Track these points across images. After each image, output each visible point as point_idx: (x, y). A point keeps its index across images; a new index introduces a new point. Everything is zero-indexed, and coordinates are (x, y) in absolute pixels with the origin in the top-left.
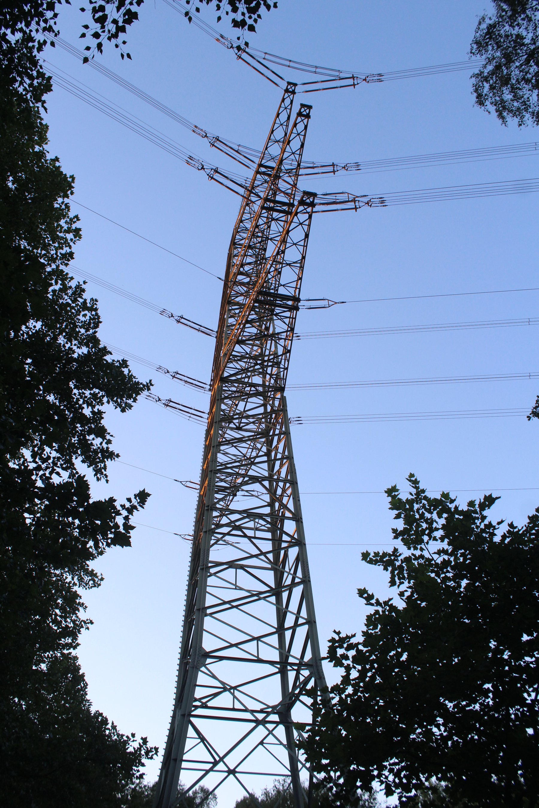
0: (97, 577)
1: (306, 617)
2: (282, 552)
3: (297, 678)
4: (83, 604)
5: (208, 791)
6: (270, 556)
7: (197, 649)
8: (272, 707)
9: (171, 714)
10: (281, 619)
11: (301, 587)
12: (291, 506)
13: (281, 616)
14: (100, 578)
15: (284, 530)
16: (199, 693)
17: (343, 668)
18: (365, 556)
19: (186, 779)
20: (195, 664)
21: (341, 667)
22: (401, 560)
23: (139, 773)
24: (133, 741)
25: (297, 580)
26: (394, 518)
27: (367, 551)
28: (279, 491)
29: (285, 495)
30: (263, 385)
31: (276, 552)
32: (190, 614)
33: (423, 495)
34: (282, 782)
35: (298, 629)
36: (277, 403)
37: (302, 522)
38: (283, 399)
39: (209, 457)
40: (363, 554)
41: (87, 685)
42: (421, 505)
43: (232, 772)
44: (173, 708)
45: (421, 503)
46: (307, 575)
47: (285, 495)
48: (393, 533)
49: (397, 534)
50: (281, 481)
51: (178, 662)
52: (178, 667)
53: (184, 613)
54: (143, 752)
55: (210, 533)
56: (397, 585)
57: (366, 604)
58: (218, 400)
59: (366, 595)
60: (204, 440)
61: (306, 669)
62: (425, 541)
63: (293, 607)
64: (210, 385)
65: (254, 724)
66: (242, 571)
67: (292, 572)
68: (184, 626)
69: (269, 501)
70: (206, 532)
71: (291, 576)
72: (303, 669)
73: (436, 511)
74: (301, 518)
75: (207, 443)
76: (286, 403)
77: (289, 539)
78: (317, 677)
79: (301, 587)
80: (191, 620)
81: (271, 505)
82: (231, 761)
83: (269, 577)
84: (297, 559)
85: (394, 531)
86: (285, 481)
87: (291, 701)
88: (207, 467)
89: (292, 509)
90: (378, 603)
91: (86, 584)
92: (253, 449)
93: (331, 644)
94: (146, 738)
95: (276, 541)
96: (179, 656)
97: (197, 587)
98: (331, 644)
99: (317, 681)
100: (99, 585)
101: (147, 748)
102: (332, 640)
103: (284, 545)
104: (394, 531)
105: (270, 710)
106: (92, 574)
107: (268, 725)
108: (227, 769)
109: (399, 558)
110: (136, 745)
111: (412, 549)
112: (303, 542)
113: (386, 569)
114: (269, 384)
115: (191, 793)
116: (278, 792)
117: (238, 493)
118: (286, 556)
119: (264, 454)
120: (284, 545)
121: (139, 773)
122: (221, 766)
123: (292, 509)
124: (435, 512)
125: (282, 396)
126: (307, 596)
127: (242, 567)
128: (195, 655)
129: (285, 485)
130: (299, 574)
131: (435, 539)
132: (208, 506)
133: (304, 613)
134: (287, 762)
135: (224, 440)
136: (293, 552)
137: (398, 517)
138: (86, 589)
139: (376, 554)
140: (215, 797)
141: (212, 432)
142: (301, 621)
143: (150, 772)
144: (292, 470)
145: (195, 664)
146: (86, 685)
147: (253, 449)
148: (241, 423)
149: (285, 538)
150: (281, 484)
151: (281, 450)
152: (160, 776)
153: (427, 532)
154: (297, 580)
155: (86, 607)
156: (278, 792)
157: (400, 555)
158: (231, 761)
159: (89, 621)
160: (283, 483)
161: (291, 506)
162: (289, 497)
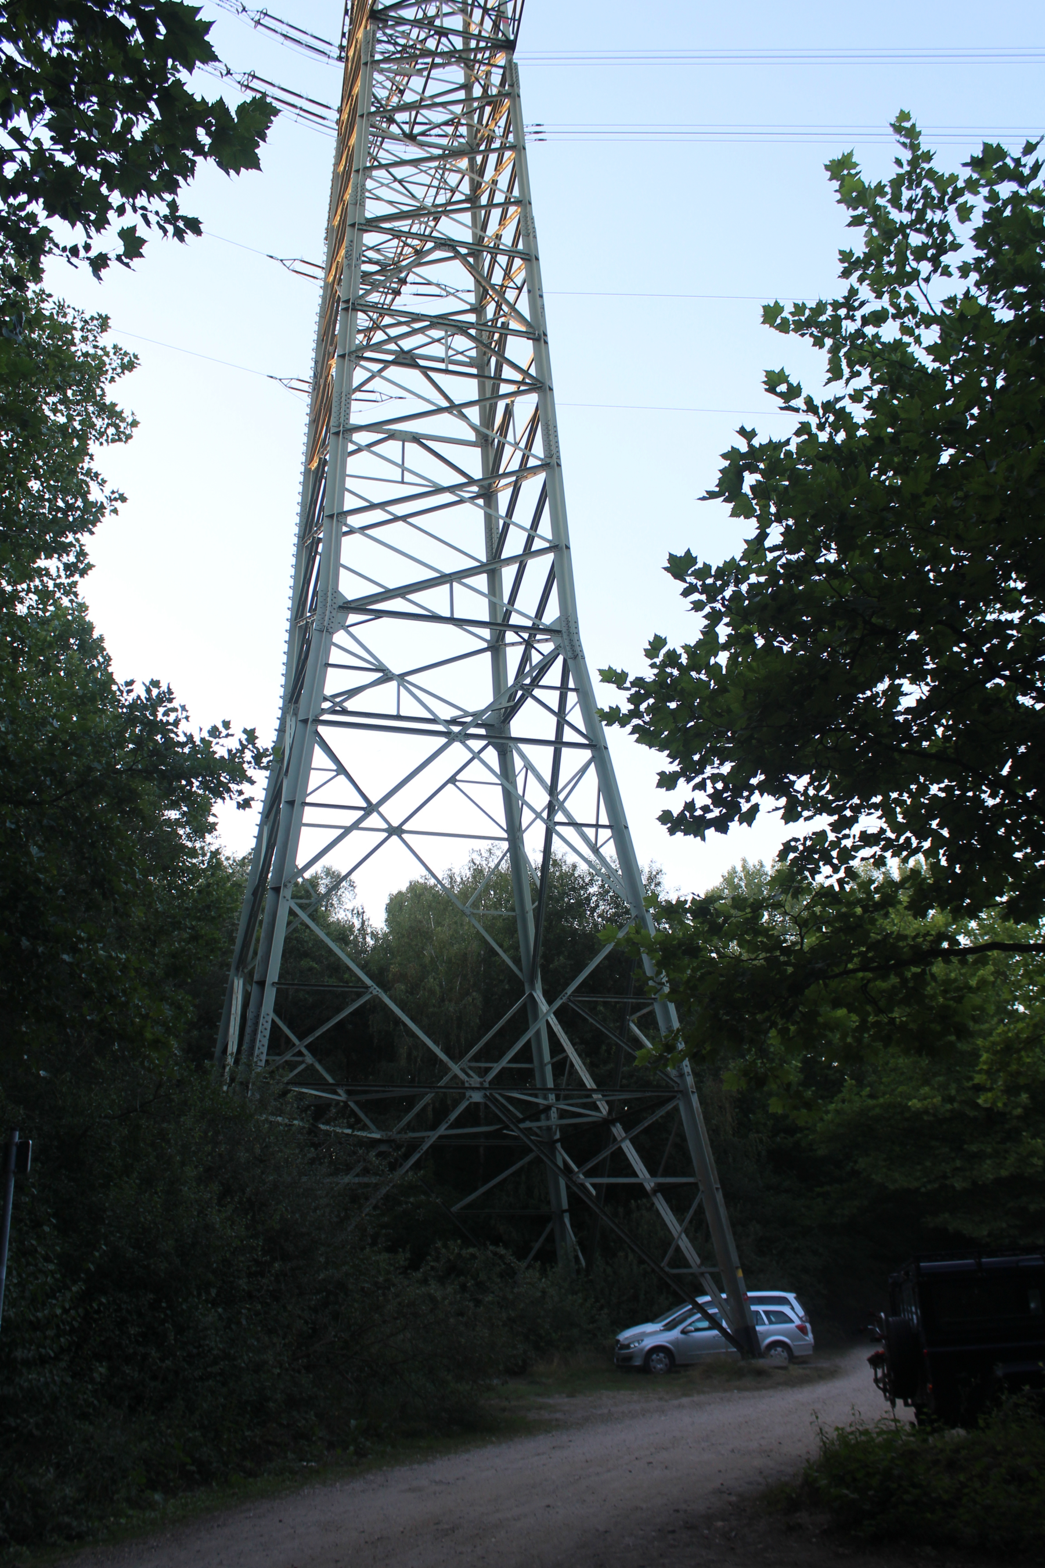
0: (123, 420)
1: (550, 537)
2: (501, 406)
3: (526, 658)
4: (97, 475)
5: (339, 875)
7: (329, 594)
8: (473, 715)
9: (276, 724)
10: (495, 546)
11: (541, 477)
12: (523, 306)
13: (496, 539)
14: (130, 420)
16: (335, 682)
17: (754, 520)
18: (771, 314)
19: (308, 845)
20: (326, 624)
21: (747, 517)
22: (863, 317)
23: (243, 797)
24: (228, 735)
25: (532, 462)
26: (849, 225)
27: (776, 303)
28: (497, 278)
30: (466, 34)
31: (487, 404)
32: (311, 528)
33: (926, 166)
34: (486, 854)
35: (532, 564)
36: (496, 79)
38: (511, 69)
39: (347, 197)
40: (766, 308)
41: (110, 659)
42: (919, 191)
43: (395, 831)
44: (279, 713)
45: (918, 185)
46: (554, 451)
47: (511, 285)
48: (842, 261)
49: (850, 264)
50: (504, 252)
51: (287, 625)
52: (286, 636)
53: (296, 530)
54: (248, 755)
55: (353, 358)
56: (845, 378)
57: (781, 409)
58: (366, 64)
59: (783, 388)
60: (333, 161)
61: (546, 640)
62: (924, 275)
63: (524, 514)
64: (341, 48)
65: (443, 740)
66: (415, 446)
67: (522, 445)
68: (298, 556)
72: (539, 641)
73: (954, 206)
74: (545, 335)
75: (341, 168)
76: (518, 80)
77: (519, 377)
78: (570, 654)
79: (541, 477)
80: (312, 542)
81: (478, 309)
82: (394, 811)
83: (472, 462)
84: (534, 421)
85: (845, 256)
86: (512, 254)
87: (512, 704)
88: (343, 221)
90: (811, 407)
91: (102, 434)
92: (438, 188)
93: (727, 463)
94: (253, 731)
96: (288, 614)
97: (322, 477)
98: (727, 463)
99: (569, 661)
100: (129, 437)
101: (257, 749)
102: (732, 455)
103: (505, 389)
104: (845, 256)
105: (469, 719)
106: (111, 412)
107: (471, 743)
108: (385, 826)
109: (858, 314)
110: (233, 744)
111: (886, 296)
112: (548, 383)
113: (819, 343)
114: (480, 32)
115: (307, 875)
116: (478, 872)
117: (404, 289)
118: (509, 412)
119: (463, 197)
120: (505, 389)
121: (243, 797)
122: (374, 820)
124: (952, 208)
125: (510, 61)
126: (552, 495)
128: (325, 606)
129: (510, 264)
130: (538, 448)
131: (946, 272)
132: (347, 301)
133: (545, 528)
134: (500, 814)
135: (376, 163)
136: (525, 406)
137: (856, 221)
138: (101, 444)
139: (799, 309)
140: (352, 886)
141: (352, 141)
142: (538, 544)
143: (233, 831)
144: (526, 229)
145: (326, 624)
146: (108, 659)
147: (438, 188)
148: (415, 123)
149: (508, 373)
150: (503, 260)
151: (503, 182)
152: (259, 838)
153: (930, 253)
154: (532, 462)
155: (104, 481)
156: (478, 872)
157: (862, 304)
158: (394, 811)
159: (116, 495)
160: (506, 259)
161: (523, 306)
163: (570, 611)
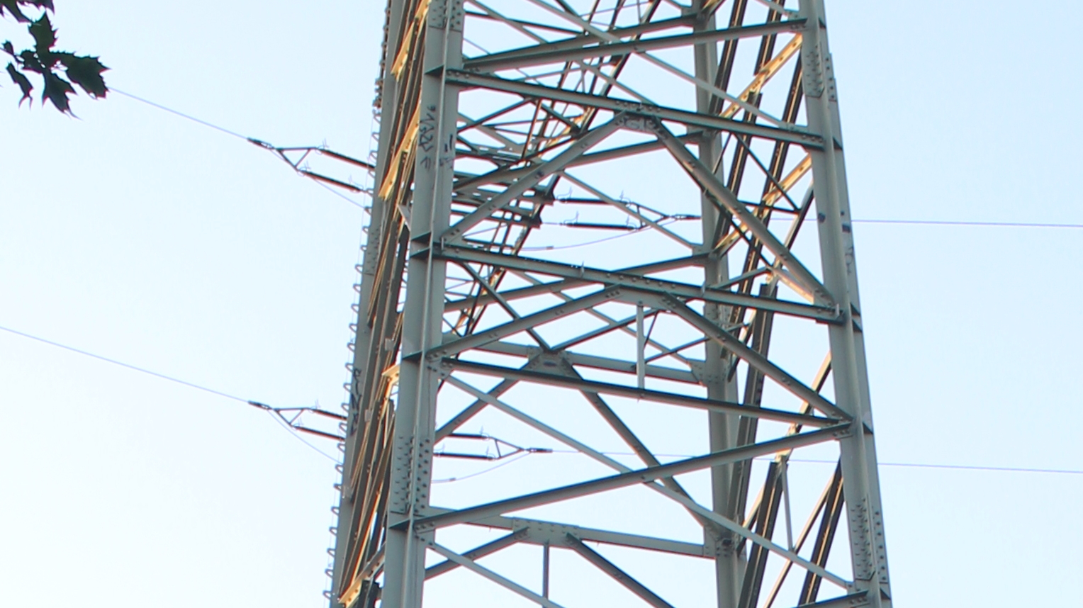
2: (760, 468)
6: (700, 484)
12: (808, 250)
15: (772, 357)
28: (752, 188)
29: (783, 203)
31: (730, 463)
37: (858, 330)
46: (875, 567)
47: (783, 203)
50: (765, 132)
55: (436, 364)
67: (806, 553)
69: (699, 239)
70: (413, 360)
71: (804, 572)
77: (797, 405)
89: (815, 267)
95: (736, 419)
112: (862, 419)
117: (548, 213)
118: (776, 482)
120: (767, 430)
123: (815, 267)
127: (575, 539)
132: (424, 240)
144: (814, 82)
149: (774, 395)
150: (763, 148)
161: (808, 250)
162: (801, 213)
163: (857, 395)
